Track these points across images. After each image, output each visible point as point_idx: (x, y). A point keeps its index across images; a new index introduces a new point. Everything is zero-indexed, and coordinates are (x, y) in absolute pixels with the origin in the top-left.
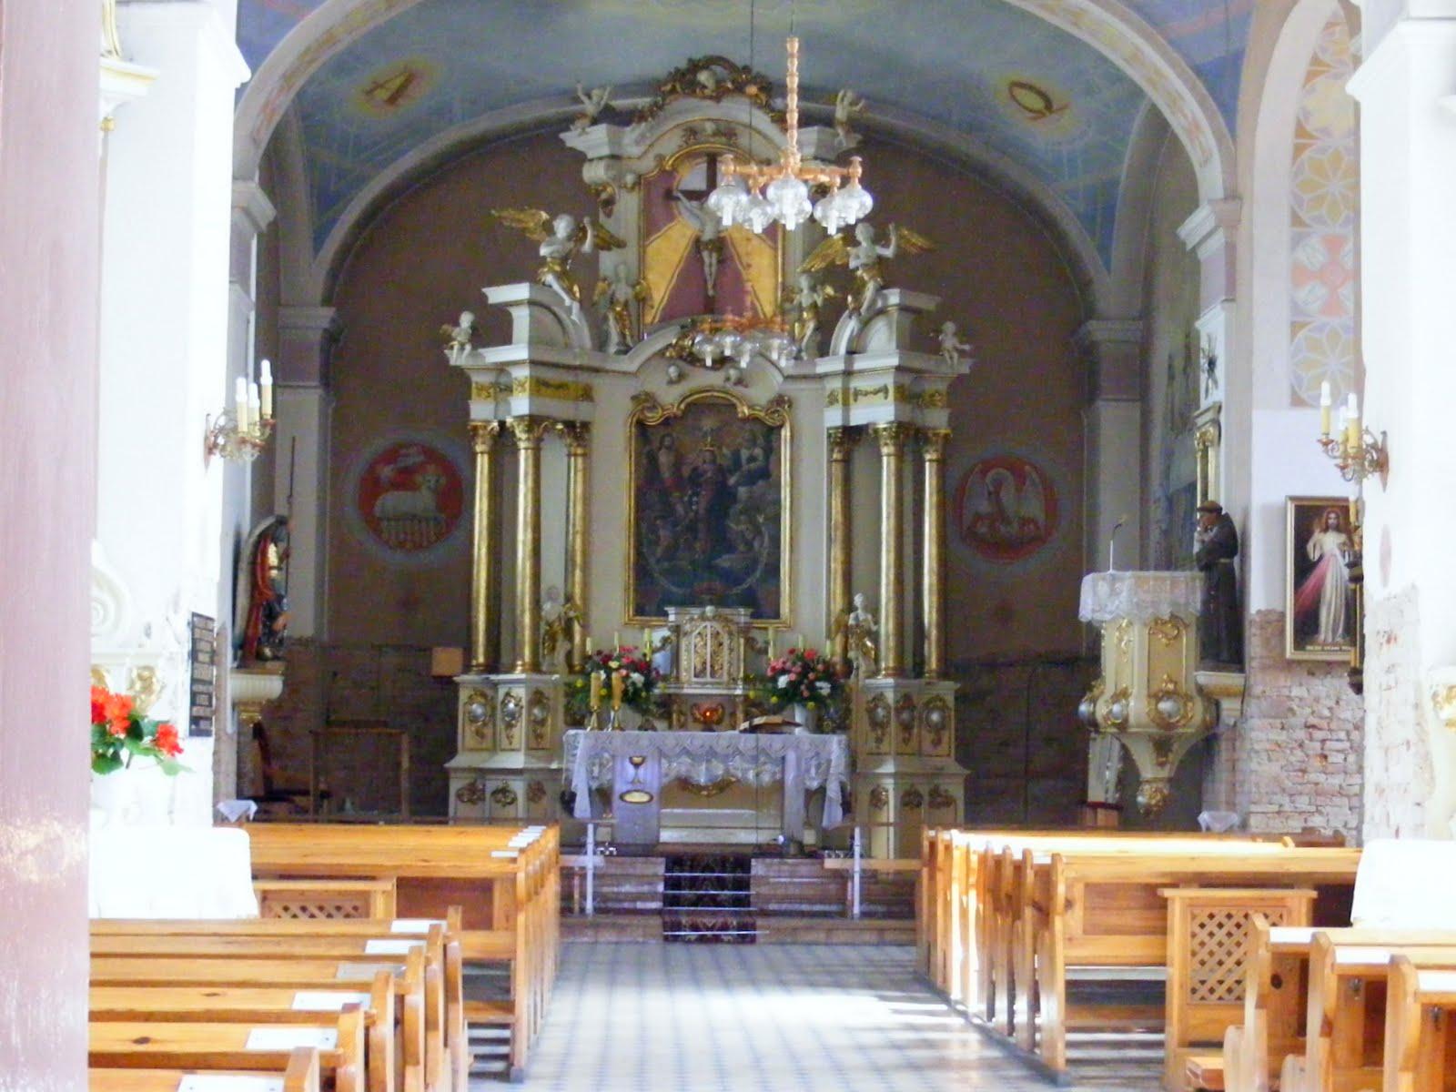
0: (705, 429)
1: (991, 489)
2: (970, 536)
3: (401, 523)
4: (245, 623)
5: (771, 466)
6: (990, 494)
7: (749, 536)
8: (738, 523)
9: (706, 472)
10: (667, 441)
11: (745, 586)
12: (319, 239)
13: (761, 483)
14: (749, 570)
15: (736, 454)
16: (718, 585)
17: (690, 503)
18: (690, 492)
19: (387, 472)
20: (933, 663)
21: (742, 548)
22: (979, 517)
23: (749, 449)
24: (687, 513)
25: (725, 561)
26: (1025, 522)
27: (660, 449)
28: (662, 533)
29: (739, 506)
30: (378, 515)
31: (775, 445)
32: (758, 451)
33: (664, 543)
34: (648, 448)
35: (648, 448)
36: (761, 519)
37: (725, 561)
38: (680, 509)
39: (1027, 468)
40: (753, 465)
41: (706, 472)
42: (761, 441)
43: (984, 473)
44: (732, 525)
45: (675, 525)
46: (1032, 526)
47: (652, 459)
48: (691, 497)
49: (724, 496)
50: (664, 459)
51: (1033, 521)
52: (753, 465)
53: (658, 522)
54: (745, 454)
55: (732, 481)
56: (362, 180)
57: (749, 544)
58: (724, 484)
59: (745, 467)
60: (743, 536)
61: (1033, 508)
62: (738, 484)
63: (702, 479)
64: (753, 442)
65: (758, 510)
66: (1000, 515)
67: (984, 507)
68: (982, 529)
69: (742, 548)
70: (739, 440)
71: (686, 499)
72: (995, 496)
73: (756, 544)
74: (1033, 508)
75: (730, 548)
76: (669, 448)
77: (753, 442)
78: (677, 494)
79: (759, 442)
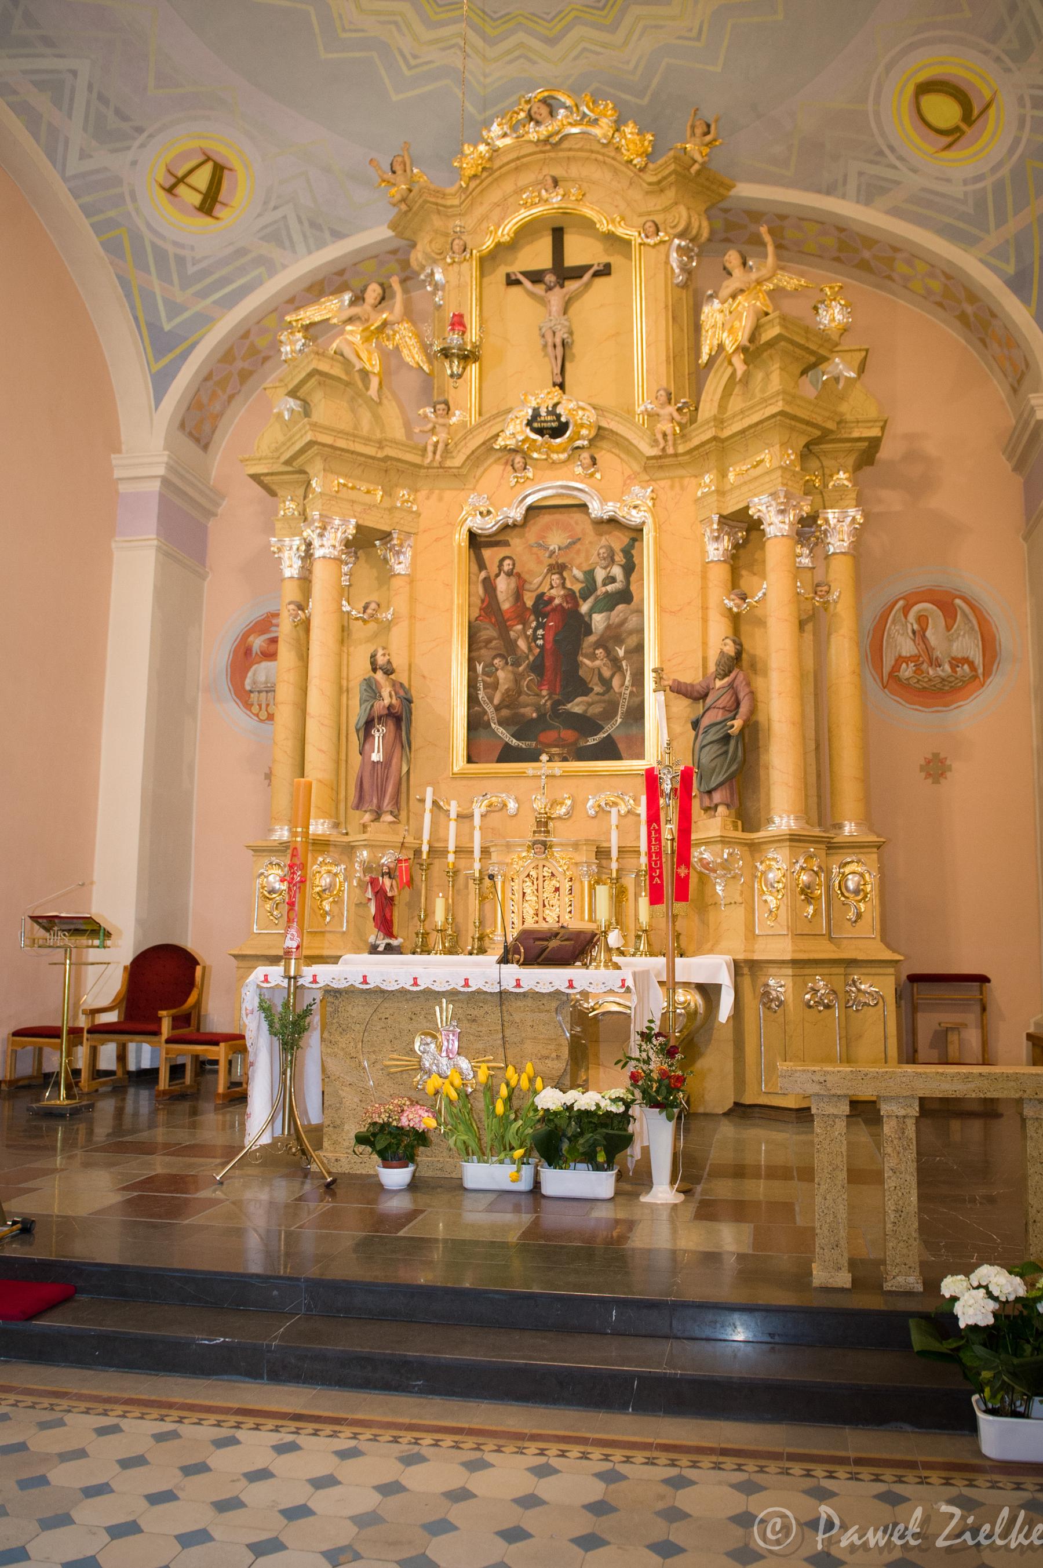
0: (551, 548)
1: (916, 627)
2: (893, 682)
3: (264, 694)
4: (356, 799)
5: (633, 588)
6: (914, 632)
7: (607, 673)
8: (593, 657)
9: (552, 599)
10: (507, 565)
11: (602, 735)
12: (161, 382)
13: (620, 607)
14: (610, 713)
15: (590, 574)
16: (569, 735)
17: (535, 638)
18: (534, 624)
19: (258, 643)
20: (586, 918)
21: (597, 689)
22: (900, 660)
23: (605, 568)
24: (530, 649)
25: (577, 706)
26: (956, 662)
27: (497, 575)
28: (501, 674)
29: (592, 639)
30: (248, 687)
31: (636, 560)
32: (617, 571)
33: (503, 687)
34: (483, 574)
35: (483, 574)
36: (621, 653)
37: (577, 706)
38: (522, 644)
39: (958, 601)
40: (610, 588)
41: (552, 599)
42: (620, 558)
43: (906, 611)
44: (587, 661)
45: (516, 664)
46: (966, 667)
47: (489, 586)
48: (535, 630)
49: (577, 626)
50: (503, 586)
51: (966, 660)
52: (610, 588)
53: (496, 661)
54: (600, 575)
55: (584, 608)
56: (205, 321)
57: (607, 683)
58: (575, 612)
59: (601, 590)
60: (600, 674)
61: (968, 646)
62: (592, 611)
63: (549, 608)
64: (611, 559)
65: (619, 641)
66: (927, 656)
67: (907, 647)
68: (907, 671)
69: (597, 689)
70: (594, 559)
71: (530, 632)
72: (920, 635)
73: (616, 683)
74: (968, 646)
75: (586, 691)
76: (509, 574)
77: (611, 559)
78: (520, 627)
79: (617, 558)
